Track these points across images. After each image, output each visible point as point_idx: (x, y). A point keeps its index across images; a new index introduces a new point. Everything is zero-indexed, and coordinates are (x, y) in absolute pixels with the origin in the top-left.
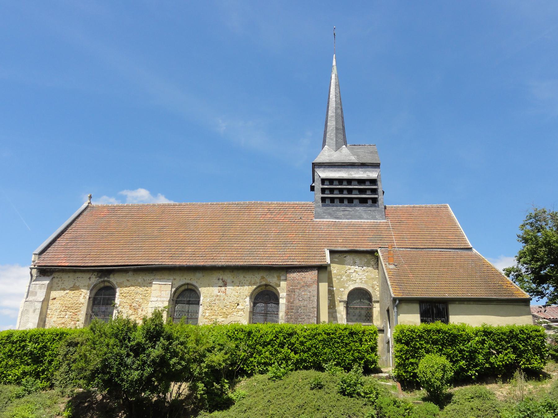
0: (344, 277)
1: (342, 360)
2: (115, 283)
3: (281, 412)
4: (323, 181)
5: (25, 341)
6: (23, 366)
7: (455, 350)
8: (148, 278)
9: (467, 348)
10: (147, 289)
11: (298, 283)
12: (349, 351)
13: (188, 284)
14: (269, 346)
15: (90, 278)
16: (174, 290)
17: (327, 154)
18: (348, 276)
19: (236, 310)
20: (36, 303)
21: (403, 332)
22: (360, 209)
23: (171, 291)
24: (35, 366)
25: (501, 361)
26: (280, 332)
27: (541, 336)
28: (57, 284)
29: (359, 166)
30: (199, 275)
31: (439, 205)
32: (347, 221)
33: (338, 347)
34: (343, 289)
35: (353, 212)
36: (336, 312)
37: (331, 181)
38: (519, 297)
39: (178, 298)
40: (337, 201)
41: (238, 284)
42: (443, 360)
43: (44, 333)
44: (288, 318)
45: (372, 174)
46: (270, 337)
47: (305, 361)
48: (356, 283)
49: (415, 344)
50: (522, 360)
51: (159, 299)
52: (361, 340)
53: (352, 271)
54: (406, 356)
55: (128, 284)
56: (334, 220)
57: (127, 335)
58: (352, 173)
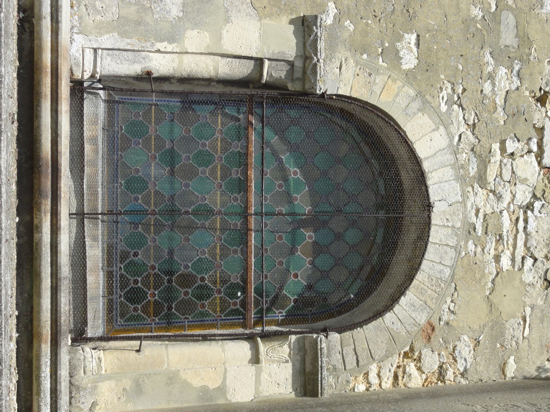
34: (409, 60)
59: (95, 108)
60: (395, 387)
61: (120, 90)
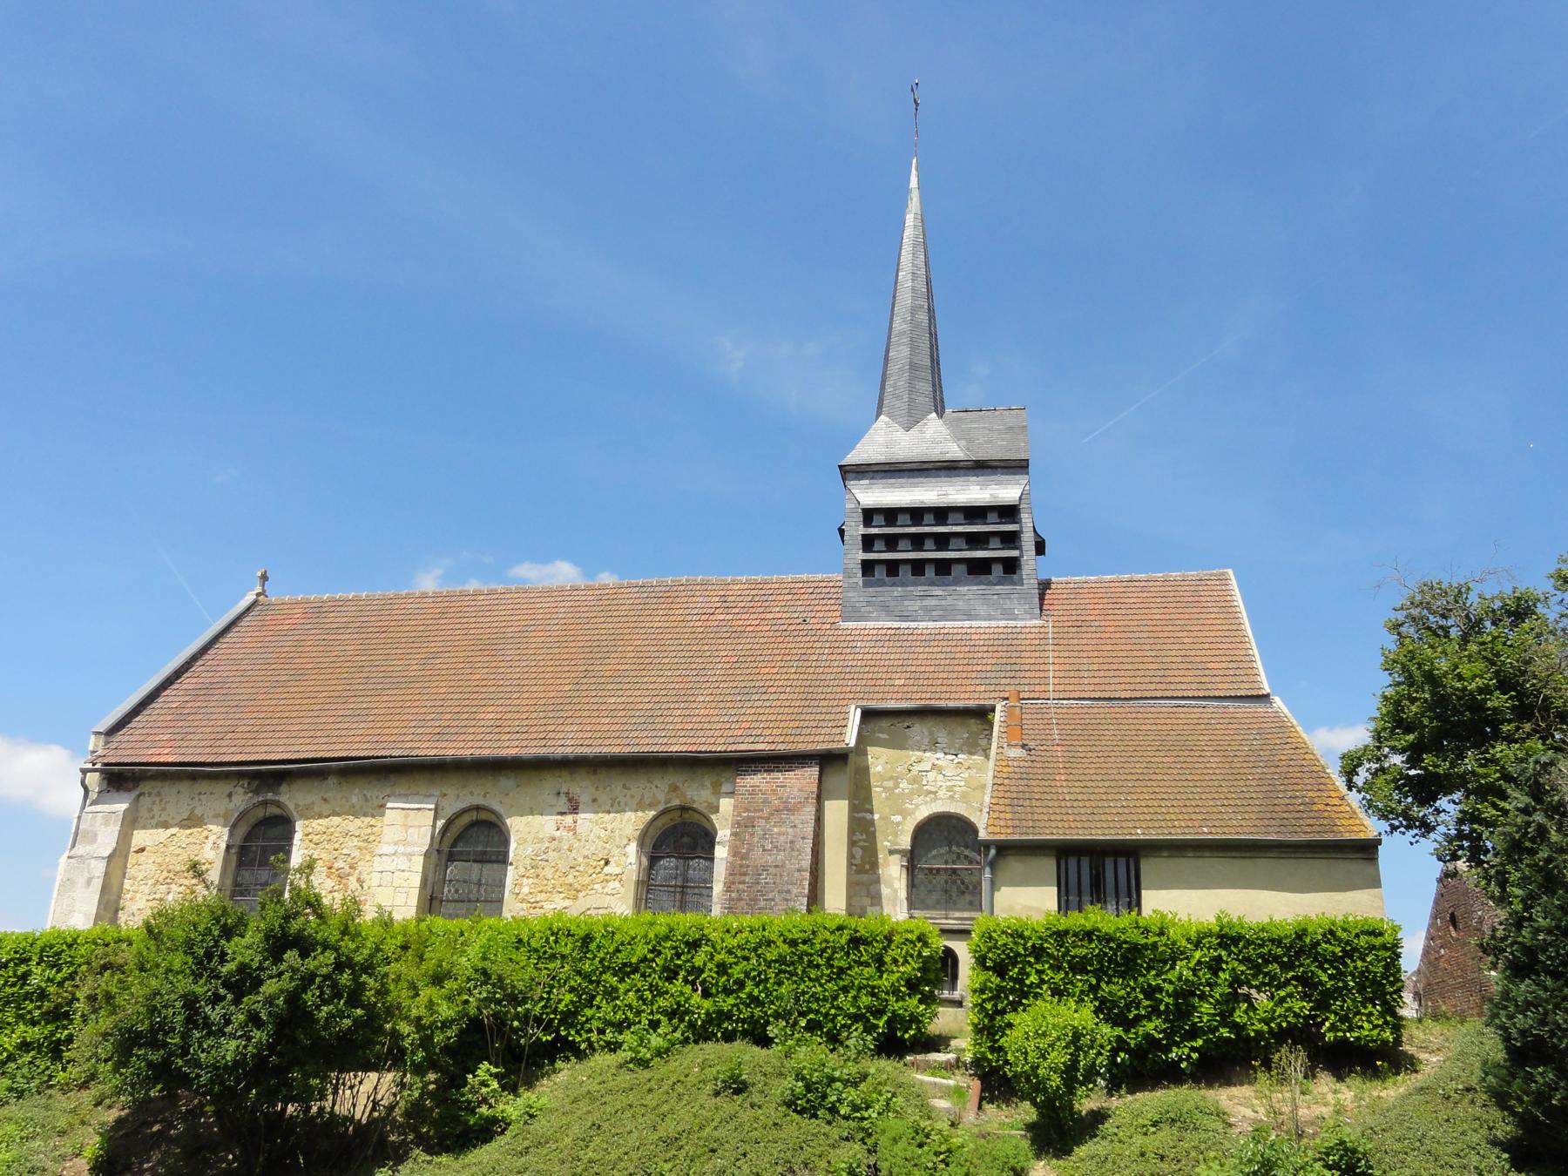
0: (904, 785)
1: (827, 1014)
2: (291, 807)
3: (613, 1157)
4: (869, 515)
5: (27, 960)
6: (22, 1027)
7: (1133, 989)
8: (375, 793)
9: (1171, 982)
10: (373, 822)
11: (766, 802)
12: (845, 990)
13: (478, 808)
14: (637, 976)
15: (230, 795)
16: (440, 823)
17: (884, 439)
18: (914, 780)
19: (601, 876)
20: (93, 862)
21: (990, 938)
22: (968, 592)
23: (434, 826)
24: (50, 1027)
25: (1266, 1022)
26: (667, 938)
27: (1384, 947)
28: (150, 810)
29: (967, 468)
30: (506, 782)
31: (1203, 573)
32: (931, 624)
33: (817, 980)
34: (899, 818)
35: (950, 600)
36: (878, 881)
37: (891, 514)
38: (1347, 836)
39: (454, 845)
40: (905, 571)
41: (608, 807)
42: (1083, 1016)
43: (75, 940)
44: (731, 899)
45: (1006, 491)
46: (642, 950)
47: (728, 1016)
48: (936, 799)
49: (1022, 972)
50: (1327, 1019)
51: (401, 849)
52: (880, 961)
53: (926, 766)
54: (995, 1005)
55: (326, 808)
56: (896, 624)
57: (216, 944)
58: (951, 490)
59: (916, 913)
60: (1350, 773)
61: (911, 906)
